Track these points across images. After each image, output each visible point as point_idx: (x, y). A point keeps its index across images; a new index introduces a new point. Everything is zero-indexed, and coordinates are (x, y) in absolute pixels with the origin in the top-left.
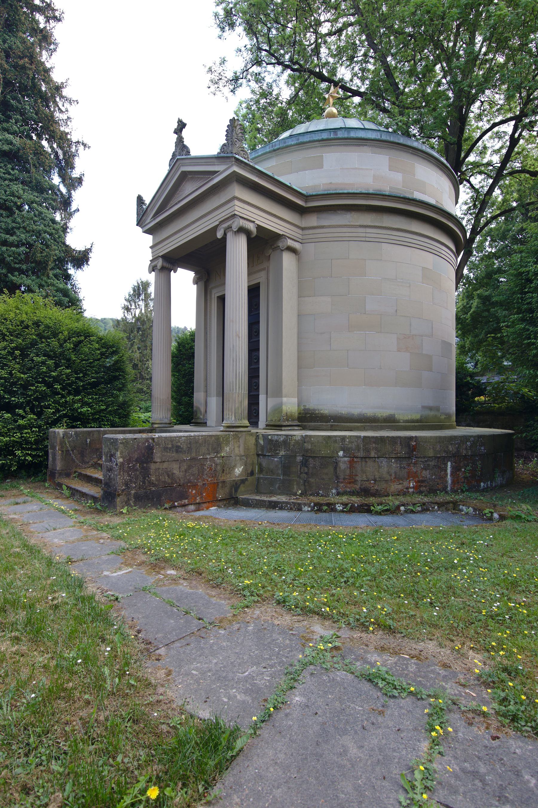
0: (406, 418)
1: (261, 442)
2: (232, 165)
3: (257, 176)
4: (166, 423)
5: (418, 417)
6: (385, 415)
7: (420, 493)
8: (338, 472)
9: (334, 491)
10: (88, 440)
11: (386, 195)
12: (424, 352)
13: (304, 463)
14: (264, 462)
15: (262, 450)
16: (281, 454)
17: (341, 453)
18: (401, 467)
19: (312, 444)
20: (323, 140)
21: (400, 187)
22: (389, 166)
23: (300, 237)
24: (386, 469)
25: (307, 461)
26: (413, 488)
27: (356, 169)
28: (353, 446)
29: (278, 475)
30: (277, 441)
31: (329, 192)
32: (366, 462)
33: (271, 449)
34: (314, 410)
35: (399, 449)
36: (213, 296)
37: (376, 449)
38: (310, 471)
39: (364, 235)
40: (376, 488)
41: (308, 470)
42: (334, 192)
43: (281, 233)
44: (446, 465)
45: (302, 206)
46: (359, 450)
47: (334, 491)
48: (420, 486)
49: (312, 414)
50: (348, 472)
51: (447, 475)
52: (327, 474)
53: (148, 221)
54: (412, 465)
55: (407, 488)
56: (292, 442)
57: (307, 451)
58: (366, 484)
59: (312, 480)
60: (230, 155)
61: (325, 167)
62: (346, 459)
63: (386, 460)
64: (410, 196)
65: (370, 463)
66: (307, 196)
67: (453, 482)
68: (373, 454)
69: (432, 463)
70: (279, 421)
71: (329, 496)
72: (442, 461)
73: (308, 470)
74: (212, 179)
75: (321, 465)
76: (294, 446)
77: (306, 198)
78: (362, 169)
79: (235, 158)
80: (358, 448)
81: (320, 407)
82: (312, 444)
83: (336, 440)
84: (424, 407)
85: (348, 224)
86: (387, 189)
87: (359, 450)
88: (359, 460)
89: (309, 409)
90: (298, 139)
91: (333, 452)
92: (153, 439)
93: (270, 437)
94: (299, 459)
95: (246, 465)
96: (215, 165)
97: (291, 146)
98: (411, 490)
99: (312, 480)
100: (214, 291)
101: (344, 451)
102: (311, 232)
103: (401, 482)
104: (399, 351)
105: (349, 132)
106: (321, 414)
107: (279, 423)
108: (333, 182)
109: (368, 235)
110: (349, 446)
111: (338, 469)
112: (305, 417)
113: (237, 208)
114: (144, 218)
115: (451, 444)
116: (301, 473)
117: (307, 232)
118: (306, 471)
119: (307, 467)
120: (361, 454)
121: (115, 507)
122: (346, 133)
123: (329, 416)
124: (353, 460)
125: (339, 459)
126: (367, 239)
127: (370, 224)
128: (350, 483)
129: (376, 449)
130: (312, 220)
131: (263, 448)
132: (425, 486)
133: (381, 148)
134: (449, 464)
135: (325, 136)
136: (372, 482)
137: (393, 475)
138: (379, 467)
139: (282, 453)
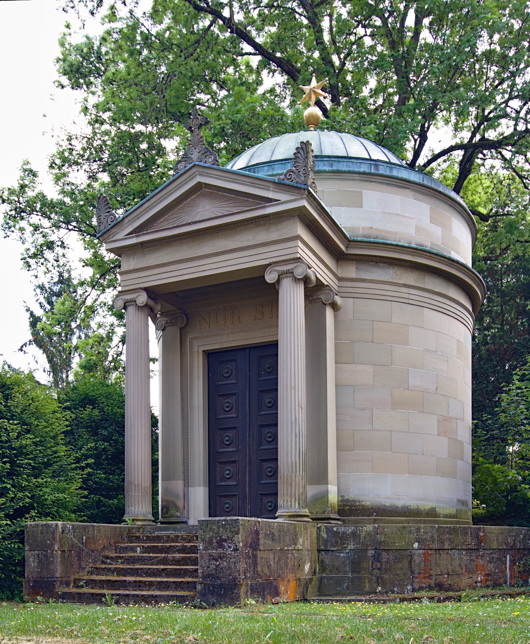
0: (445, 513)
1: (325, 536)
2: (302, 198)
3: (318, 214)
4: (150, 520)
5: (453, 511)
6: (427, 508)
7: (488, 587)
8: (413, 566)
9: (409, 587)
10: (84, 538)
11: (433, 253)
12: (459, 438)
13: (377, 558)
14: (327, 559)
15: (326, 545)
16: (349, 548)
17: (416, 545)
18: (471, 560)
19: (385, 535)
20: (364, 173)
21: (439, 244)
22: (431, 217)
23: (336, 288)
24: (458, 562)
25: (379, 555)
26: (481, 582)
27: (398, 215)
28: (428, 536)
29: (345, 572)
30: (344, 533)
31: (376, 240)
32: (440, 554)
33: (337, 543)
34: (354, 501)
35: (470, 540)
36: (196, 349)
37: (450, 539)
38: (383, 567)
39: (406, 296)
40: (449, 582)
41: (381, 565)
42: (382, 241)
43: (326, 283)
44: (506, 557)
45: (341, 249)
46: (433, 542)
47: (409, 587)
48: (487, 580)
49: (351, 506)
50: (423, 566)
51: (506, 568)
52: (401, 569)
53: (122, 235)
54: (480, 557)
55: (476, 582)
56: (363, 534)
57: (380, 543)
58: (440, 579)
59: (386, 576)
60: (303, 187)
61: (364, 206)
62: (421, 551)
63: (457, 552)
64: (448, 255)
65: (443, 554)
66: (350, 241)
67: (511, 575)
68: (446, 547)
69: (495, 556)
70: (324, 512)
71: (404, 593)
72: (503, 552)
73: (381, 565)
74: (265, 207)
75: (395, 558)
76: (365, 538)
77: (349, 242)
78: (405, 216)
79: (309, 190)
80: (433, 539)
81: (361, 498)
82: (385, 535)
83: (411, 531)
84: (459, 501)
85: (391, 280)
86: (428, 245)
87: (433, 542)
88: (433, 552)
89: (348, 500)
90: (332, 165)
91: (408, 543)
92: (259, 522)
93: (335, 529)
94: (371, 553)
95: (311, 562)
96: (269, 190)
97: (325, 172)
98: (479, 584)
99: (386, 576)
100: (196, 343)
101: (419, 542)
102: (349, 284)
103: (471, 575)
104: (439, 435)
105: (391, 168)
106: (362, 506)
107: (323, 516)
108: (375, 227)
109: (411, 297)
110: (424, 537)
111: (413, 563)
112: (343, 510)
113: (300, 251)
114: (114, 230)
115: (510, 536)
116: (373, 569)
117: (345, 284)
118: (379, 566)
119: (380, 562)
120: (435, 546)
121: (238, 598)
122: (388, 169)
123: (372, 509)
124: (428, 552)
125: (414, 552)
126: (411, 302)
127: (413, 284)
128: (425, 578)
129: (450, 539)
130: (351, 271)
131: (326, 542)
132: (491, 580)
133: (423, 194)
134: (508, 557)
135: (364, 168)
136: (446, 576)
137: (464, 568)
138: (452, 560)
139: (351, 547)
